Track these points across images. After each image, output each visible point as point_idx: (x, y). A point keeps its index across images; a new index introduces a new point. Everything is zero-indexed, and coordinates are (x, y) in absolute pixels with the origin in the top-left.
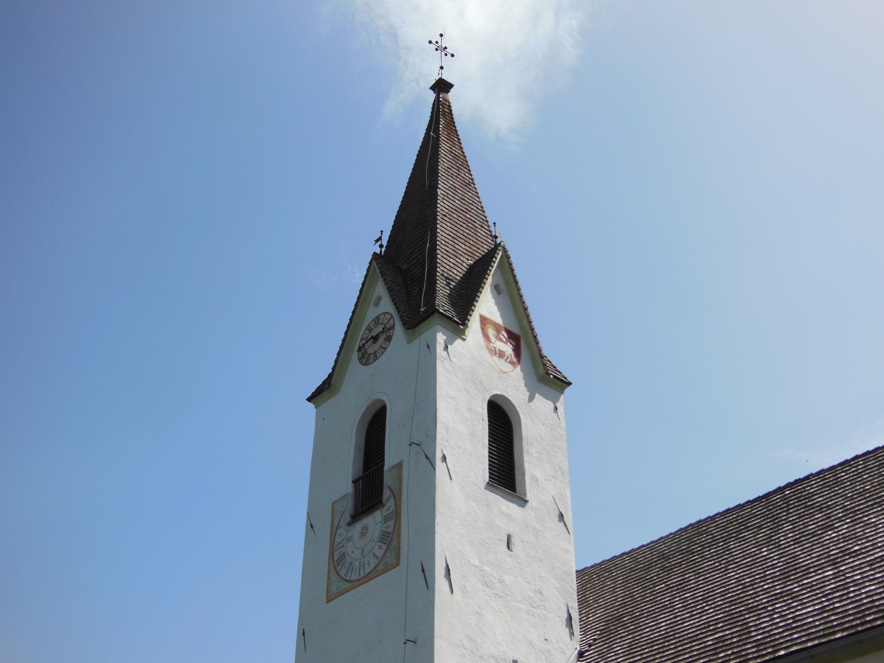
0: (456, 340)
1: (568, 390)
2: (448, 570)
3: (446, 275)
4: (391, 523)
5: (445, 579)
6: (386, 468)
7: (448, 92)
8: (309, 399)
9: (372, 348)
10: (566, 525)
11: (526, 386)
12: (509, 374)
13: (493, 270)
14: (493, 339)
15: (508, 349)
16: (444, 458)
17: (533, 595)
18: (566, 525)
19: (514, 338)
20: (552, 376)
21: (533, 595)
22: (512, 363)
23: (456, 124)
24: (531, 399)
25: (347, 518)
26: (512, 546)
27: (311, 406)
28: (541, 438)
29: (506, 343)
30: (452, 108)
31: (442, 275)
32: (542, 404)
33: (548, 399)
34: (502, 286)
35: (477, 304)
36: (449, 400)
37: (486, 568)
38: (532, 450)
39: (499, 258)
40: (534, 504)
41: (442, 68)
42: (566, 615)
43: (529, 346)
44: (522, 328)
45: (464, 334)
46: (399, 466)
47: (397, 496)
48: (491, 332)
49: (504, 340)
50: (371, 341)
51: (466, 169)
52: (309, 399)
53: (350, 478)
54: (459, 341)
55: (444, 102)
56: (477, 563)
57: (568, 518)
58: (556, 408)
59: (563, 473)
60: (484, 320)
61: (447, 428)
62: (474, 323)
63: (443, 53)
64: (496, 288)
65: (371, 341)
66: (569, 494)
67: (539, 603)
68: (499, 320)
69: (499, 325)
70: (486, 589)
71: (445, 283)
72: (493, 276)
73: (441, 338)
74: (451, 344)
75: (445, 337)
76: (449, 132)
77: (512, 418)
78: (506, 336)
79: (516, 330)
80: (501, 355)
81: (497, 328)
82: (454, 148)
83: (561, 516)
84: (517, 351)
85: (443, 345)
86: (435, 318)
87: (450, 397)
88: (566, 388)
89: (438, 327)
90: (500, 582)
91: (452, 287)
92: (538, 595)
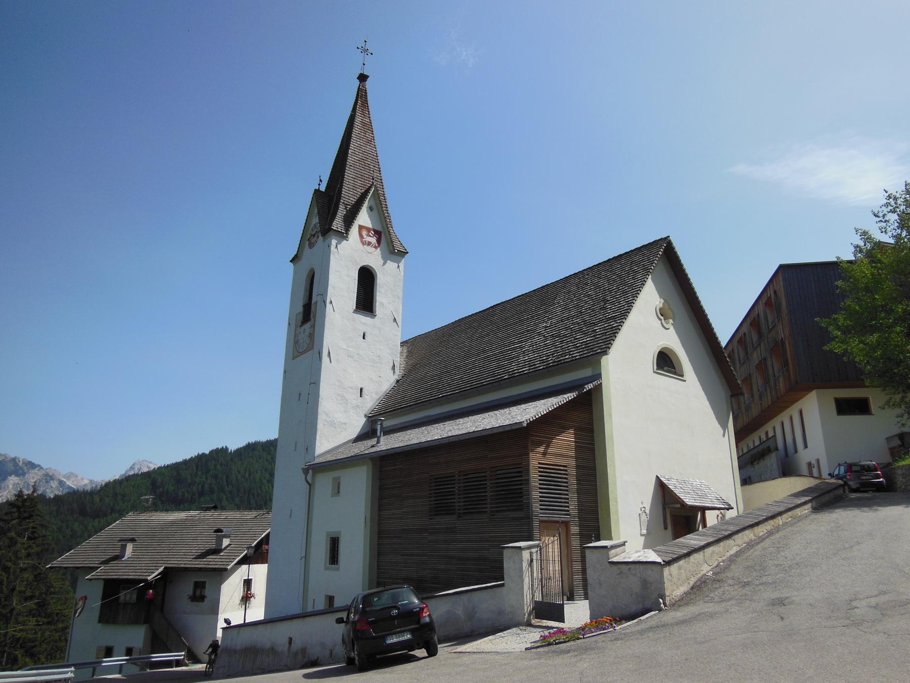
0: (342, 241)
1: (407, 256)
2: (329, 353)
3: (345, 202)
4: (312, 329)
5: (327, 357)
6: (313, 303)
7: (365, 81)
8: (291, 261)
9: (313, 240)
10: (397, 324)
11: (382, 258)
12: (374, 253)
13: (370, 196)
14: (365, 236)
15: (373, 240)
16: (331, 302)
17: (375, 358)
18: (397, 324)
19: (378, 234)
20: (396, 251)
21: (375, 358)
22: (376, 247)
23: (368, 103)
24: (384, 264)
25: (300, 324)
26: (366, 337)
27: (291, 264)
28: (388, 283)
29: (373, 237)
30: (367, 92)
31: (343, 203)
32: (392, 265)
33: (394, 262)
34: (374, 206)
35: (357, 219)
36: (336, 273)
37: (350, 349)
38: (382, 290)
39: (373, 190)
40: (380, 316)
41: (364, 64)
42: (392, 365)
43: (386, 237)
44: (383, 227)
45: (348, 238)
46: (316, 303)
47: (315, 317)
48: (364, 233)
49: (372, 235)
50: (312, 237)
51: (370, 130)
52: (291, 261)
53: (302, 305)
54: (345, 241)
55: (363, 88)
56: (346, 348)
57: (399, 320)
58: (399, 266)
59: (399, 298)
60: (361, 228)
61: (334, 287)
62: (354, 230)
63: (366, 54)
64: (371, 208)
65: (312, 237)
66: (401, 308)
67: (378, 361)
68: (370, 226)
69: (369, 228)
70: (350, 358)
71: (344, 207)
72: (369, 201)
73: (334, 242)
74: (340, 244)
75: (336, 241)
76: (363, 108)
77: (374, 274)
78: (373, 233)
79: (379, 228)
80: (369, 244)
81: (368, 230)
82: (365, 119)
83: (395, 320)
84: (379, 241)
85: (335, 245)
86: (331, 232)
87: (337, 271)
88: (405, 255)
89: (333, 236)
90: (357, 354)
91: (348, 209)
92: (378, 358)
